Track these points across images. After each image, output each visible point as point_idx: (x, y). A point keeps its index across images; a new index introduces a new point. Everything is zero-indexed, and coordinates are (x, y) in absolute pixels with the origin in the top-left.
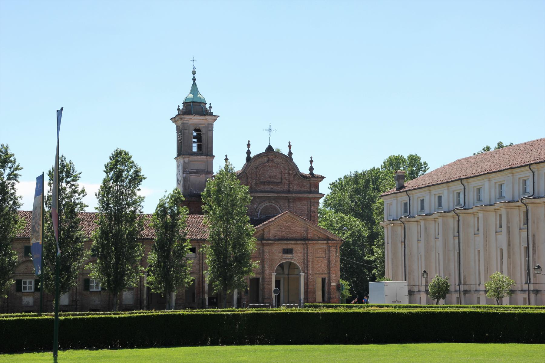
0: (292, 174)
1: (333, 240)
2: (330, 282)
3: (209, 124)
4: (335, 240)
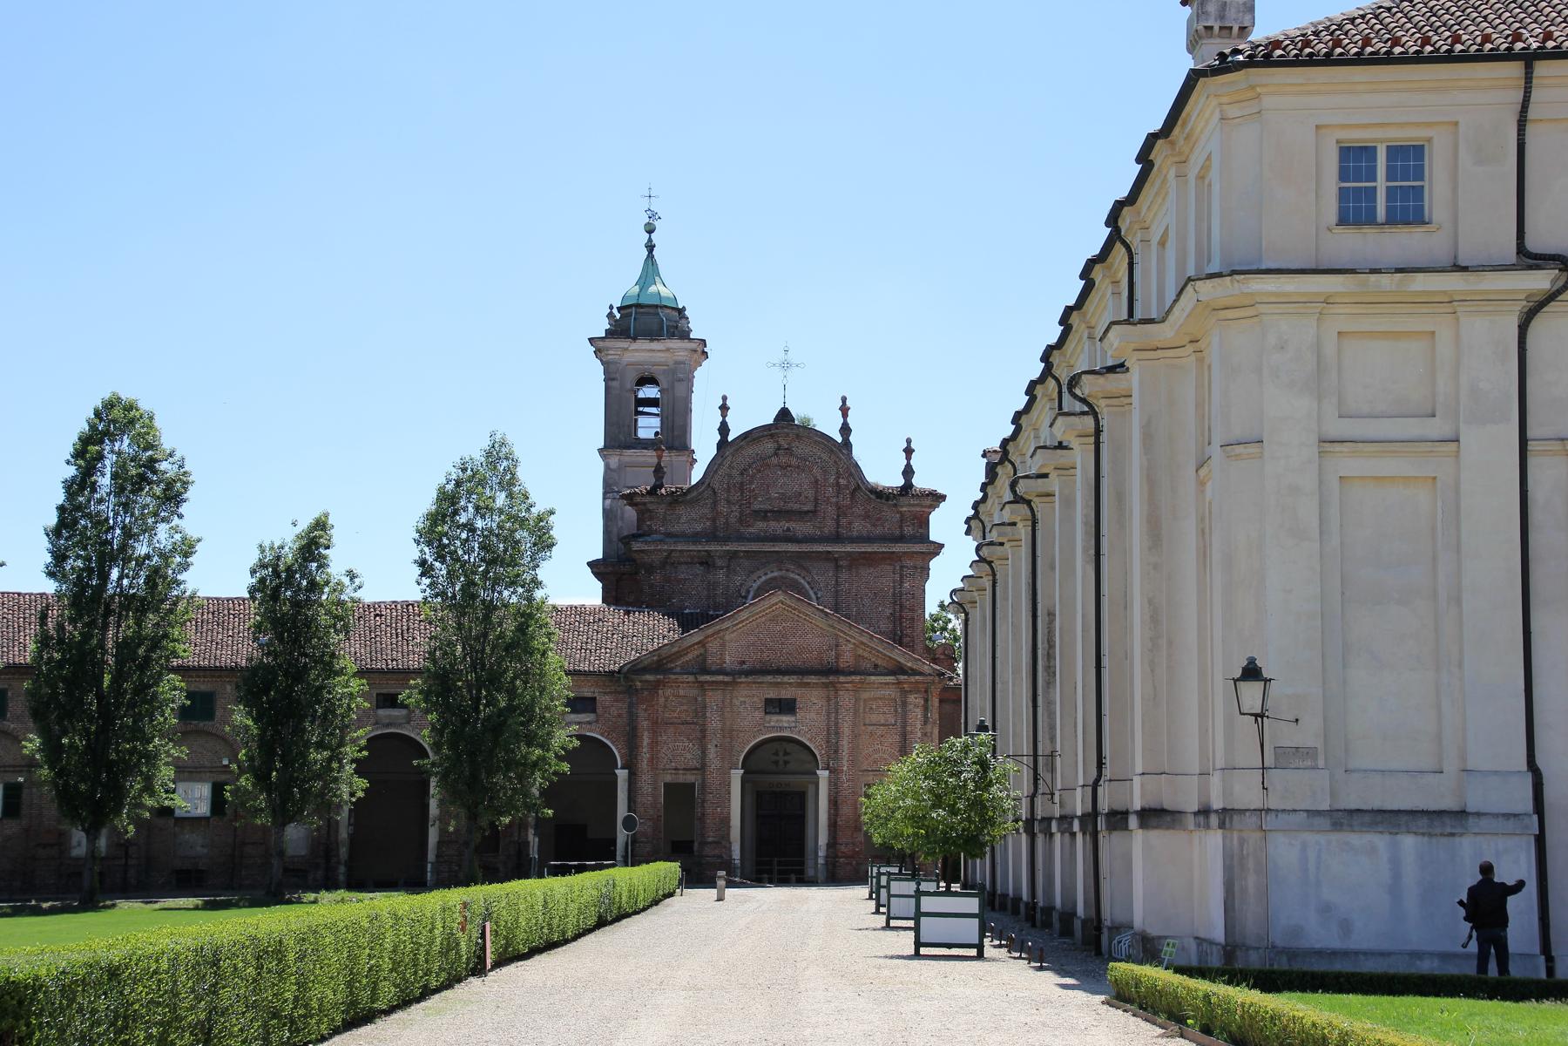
1: (915, 672)
3: (677, 363)
4: (921, 674)
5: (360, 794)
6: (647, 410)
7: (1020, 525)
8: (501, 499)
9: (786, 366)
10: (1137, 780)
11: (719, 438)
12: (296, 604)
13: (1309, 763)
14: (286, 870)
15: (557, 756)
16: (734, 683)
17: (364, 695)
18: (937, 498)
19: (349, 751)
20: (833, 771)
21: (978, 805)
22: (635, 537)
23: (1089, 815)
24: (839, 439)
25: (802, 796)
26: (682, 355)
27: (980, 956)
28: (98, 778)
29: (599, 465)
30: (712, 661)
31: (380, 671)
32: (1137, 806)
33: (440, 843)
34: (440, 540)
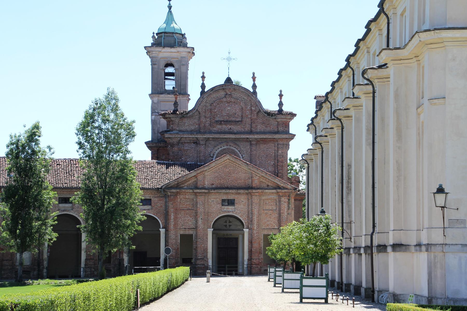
0: (255, 111)
1: (284, 188)
3: (182, 57)
4: (287, 189)
5: (55, 239)
6: (169, 77)
7: (335, 129)
8: (112, 116)
9: (229, 59)
10: (391, 233)
11: (201, 90)
12: (27, 160)
13: (462, 226)
14: (23, 271)
15: (137, 224)
16: (209, 193)
17: (55, 198)
18: (292, 115)
19: (50, 222)
20: (250, 229)
21: (325, 242)
22: (166, 131)
23: (368, 247)
24: (252, 91)
25: (237, 239)
26: (184, 54)
27: (326, 302)
28: (24, 234)
29: (149, 102)
30: (200, 184)
31: (60, 188)
32: (391, 243)
33: (86, 260)
34: (87, 134)
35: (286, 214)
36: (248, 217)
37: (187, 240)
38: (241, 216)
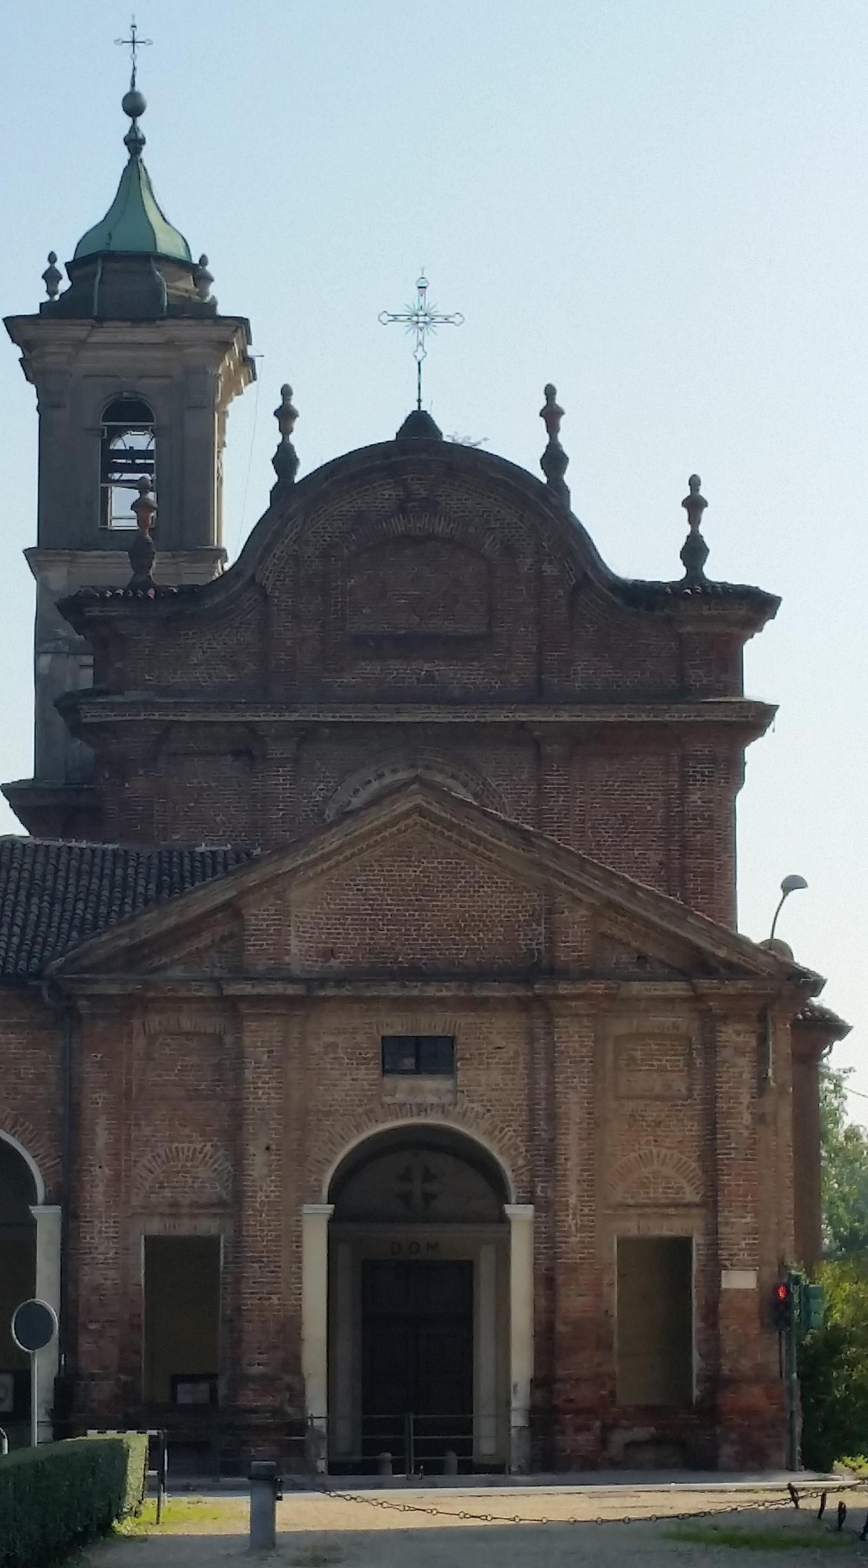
2: (715, 1267)
9: (421, 320)
11: (273, 478)
20: (547, 1208)
25: (465, 1271)
29: (26, 586)
35: (747, 1119)
36: (531, 1138)
37: (190, 1273)
38: (489, 1133)
